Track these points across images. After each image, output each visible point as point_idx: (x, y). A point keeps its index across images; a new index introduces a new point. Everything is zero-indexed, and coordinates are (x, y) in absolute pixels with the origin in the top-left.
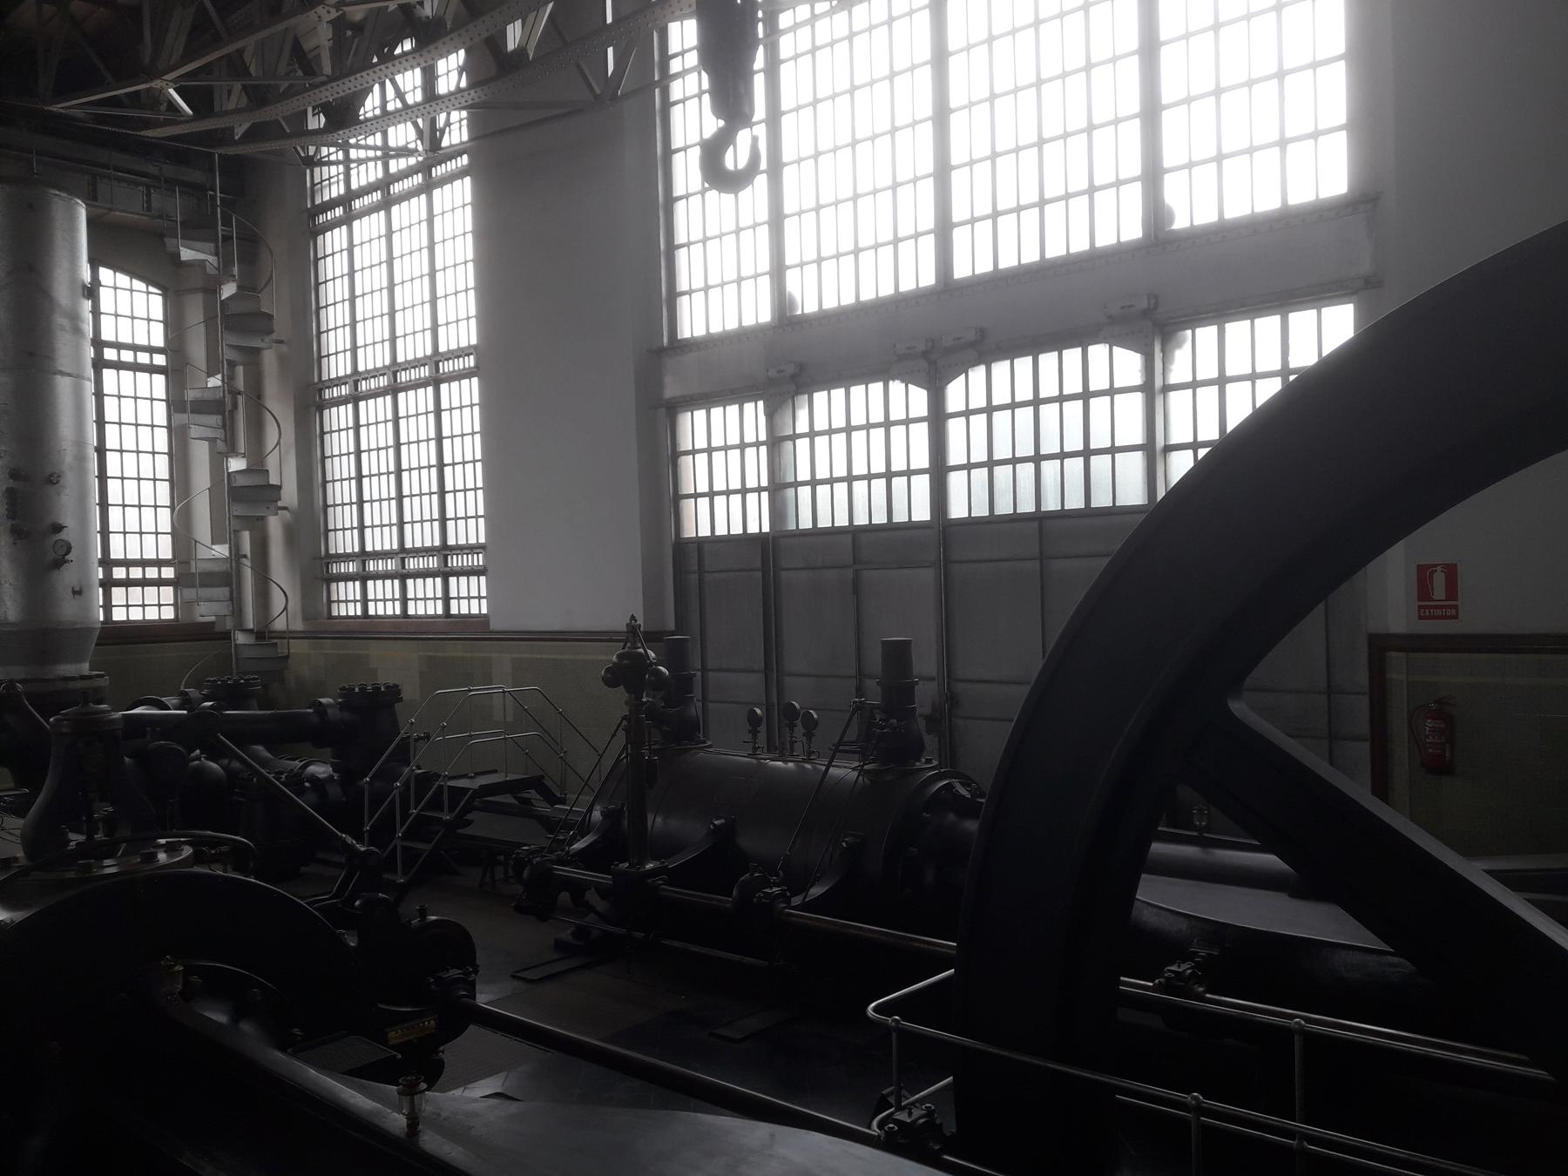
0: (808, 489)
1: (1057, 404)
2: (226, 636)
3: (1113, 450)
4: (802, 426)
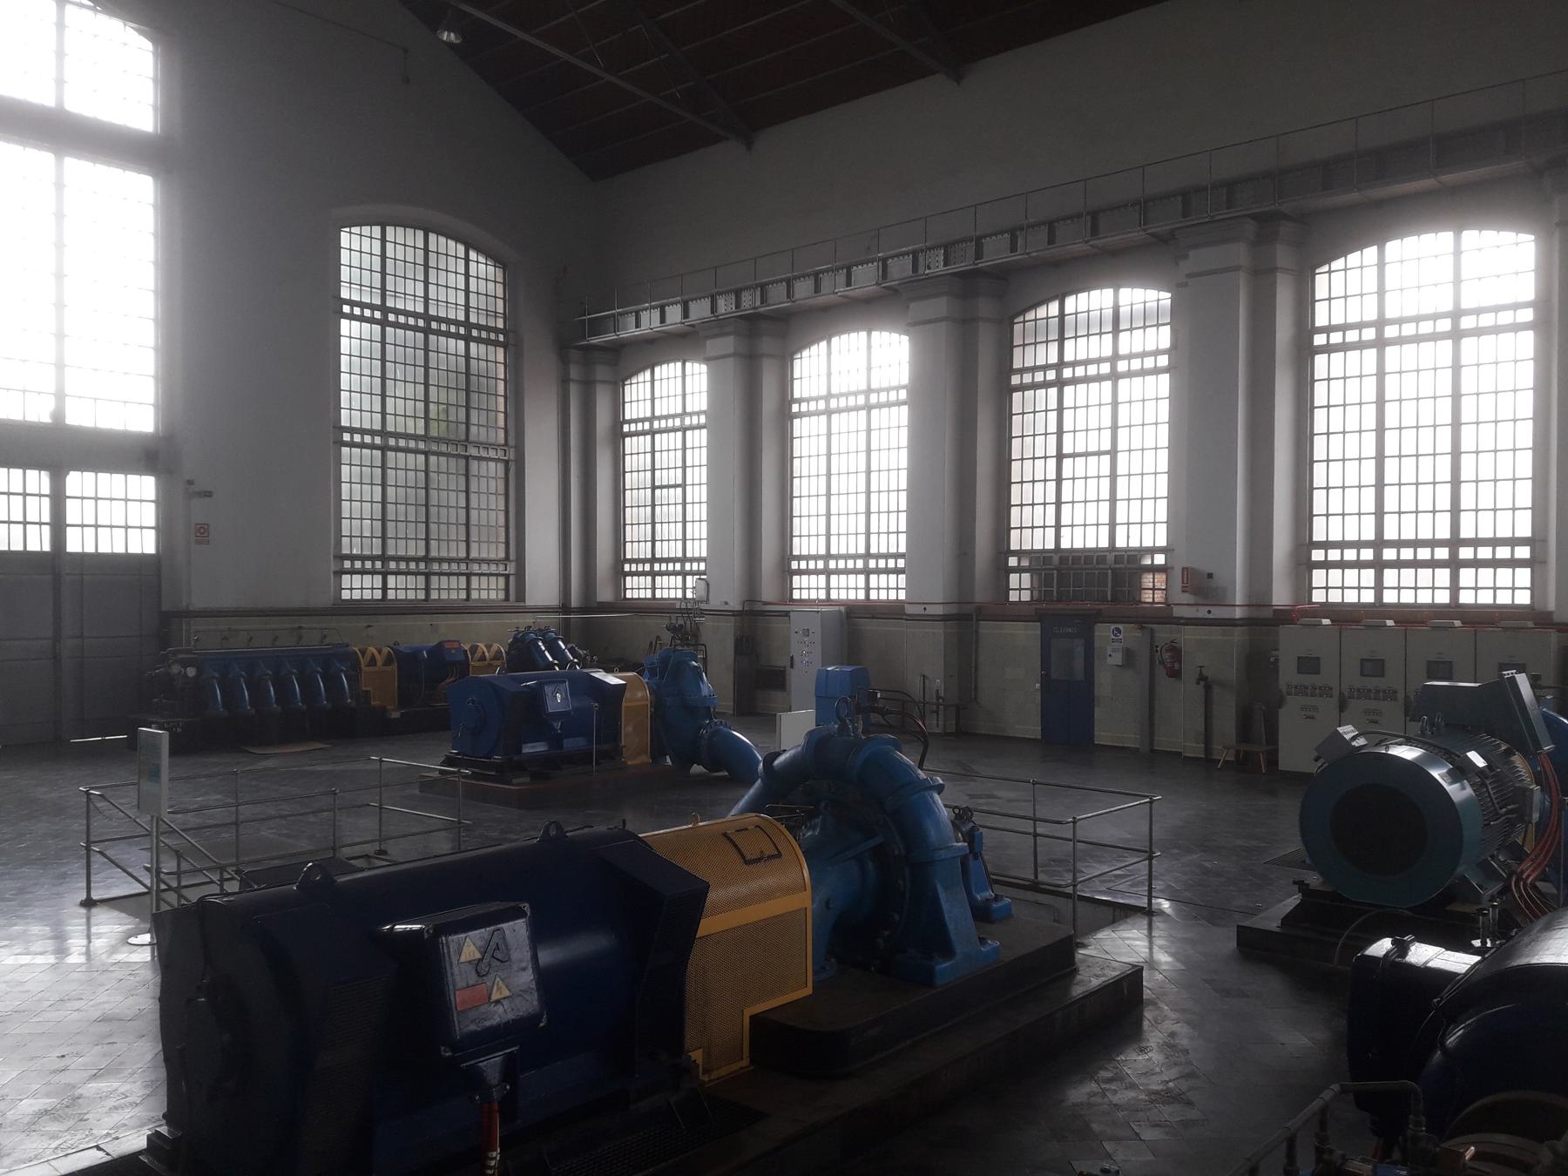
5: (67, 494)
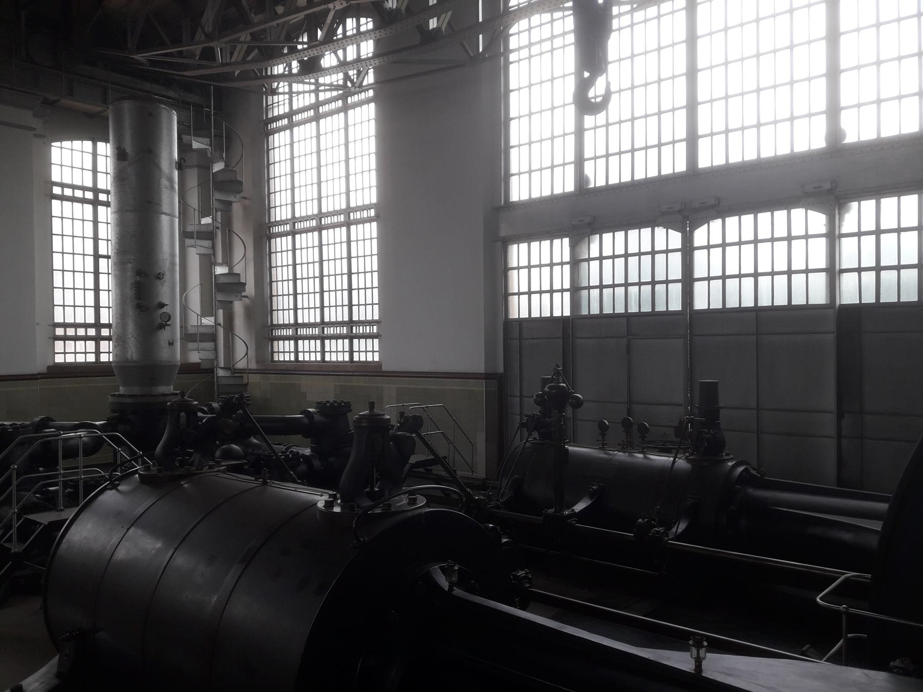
0: (597, 291)
1: (770, 243)
2: (211, 371)
3: (807, 271)
4: (595, 252)
5: (616, 233)
